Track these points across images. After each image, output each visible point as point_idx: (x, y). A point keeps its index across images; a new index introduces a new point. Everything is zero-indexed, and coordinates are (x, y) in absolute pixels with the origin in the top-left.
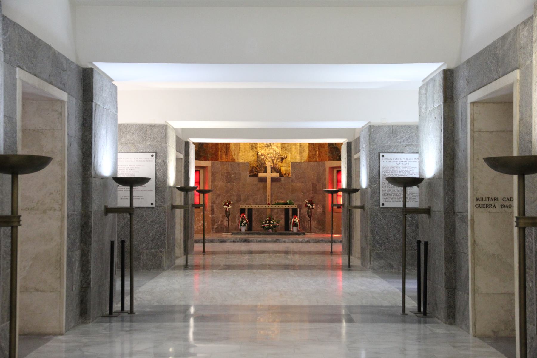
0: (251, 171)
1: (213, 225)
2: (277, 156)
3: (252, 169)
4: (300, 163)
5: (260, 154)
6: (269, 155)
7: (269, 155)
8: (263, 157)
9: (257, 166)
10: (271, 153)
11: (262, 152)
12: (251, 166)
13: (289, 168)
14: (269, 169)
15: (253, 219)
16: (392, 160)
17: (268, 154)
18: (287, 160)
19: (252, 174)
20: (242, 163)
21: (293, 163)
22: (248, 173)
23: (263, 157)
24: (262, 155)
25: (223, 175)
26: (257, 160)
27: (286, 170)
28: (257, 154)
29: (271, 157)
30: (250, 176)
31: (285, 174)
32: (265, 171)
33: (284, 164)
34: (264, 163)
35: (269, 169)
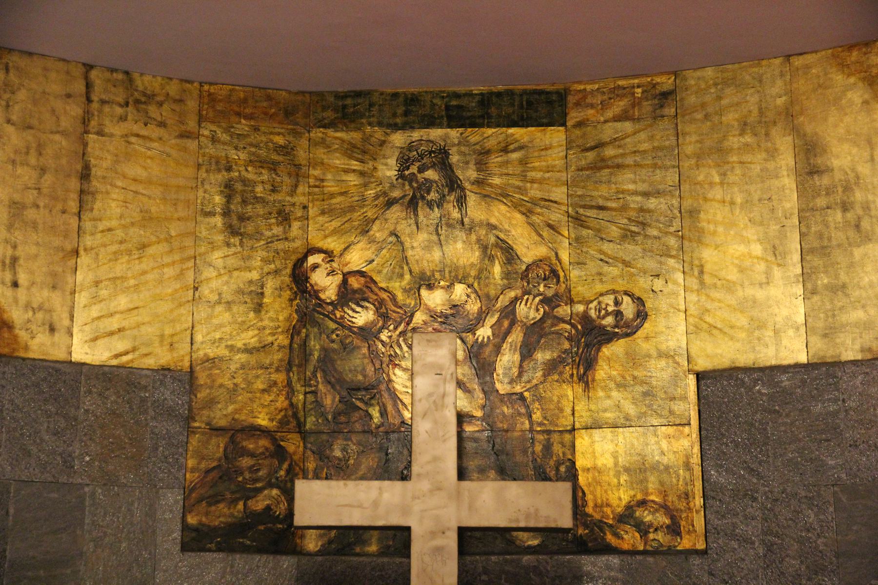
0: (223, 480)
1: (634, 234)
2: (528, 311)
3: (234, 450)
4: (820, 372)
5: (326, 283)
6: (435, 299)
7: (435, 299)
8: (363, 317)
9: (292, 420)
10: (457, 276)
11: (356, 259)
12: (221, 415)
13: (674, 446)
14: (435, 448)
15: (511, 131)
16: (629, 161)
17: (426, 281)
18: (640, 342)
19: (223, 514)
20: (103, 375)
21: (732, 373)
22: (172, 499)
23: (363, 317)
24: (348, 295)
25: (386, 220)
26: (296, 357)
27: (638, 470)
28: (300, 278)
29: (451, 320)
30: (196, 540)
31: (627, 516)
32: (395, 466)
33: (609, 400)
34: (375, 390)
35: (435, 448)
